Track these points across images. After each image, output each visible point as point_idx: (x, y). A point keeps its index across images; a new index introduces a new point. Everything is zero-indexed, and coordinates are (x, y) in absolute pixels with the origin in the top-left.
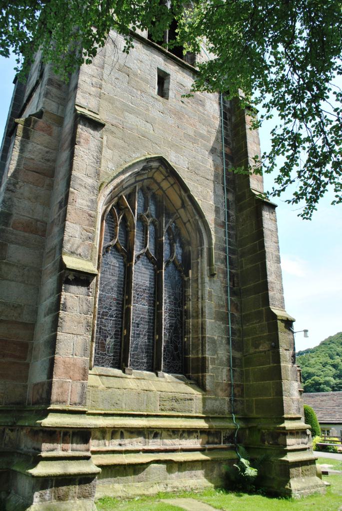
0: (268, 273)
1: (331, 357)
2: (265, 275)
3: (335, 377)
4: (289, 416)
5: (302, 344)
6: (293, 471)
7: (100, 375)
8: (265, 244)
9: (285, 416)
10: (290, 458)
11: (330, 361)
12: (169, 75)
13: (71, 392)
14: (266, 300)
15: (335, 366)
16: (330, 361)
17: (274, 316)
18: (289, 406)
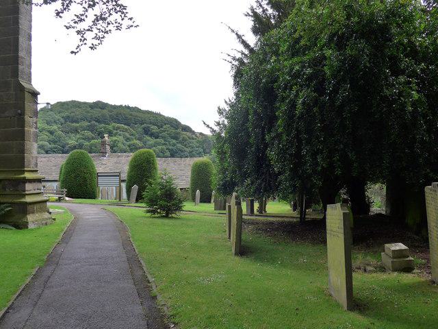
0: (20, 49)
1: (48, 123)
2: (17, 50)
3: (49, 142)
4: (29, 169)
5: (42, 102)
6: (29, 207)
7: (239, 37)
8: (20, 21)
9: (26, 169)
10: (28, 199)
11: (47, 127)
12: (236, 254)
13: (400, 258)
14: (15, 73)
15: (51, 133)
16: (47, 127)
17: (22, 89)
18: (29, 161)
